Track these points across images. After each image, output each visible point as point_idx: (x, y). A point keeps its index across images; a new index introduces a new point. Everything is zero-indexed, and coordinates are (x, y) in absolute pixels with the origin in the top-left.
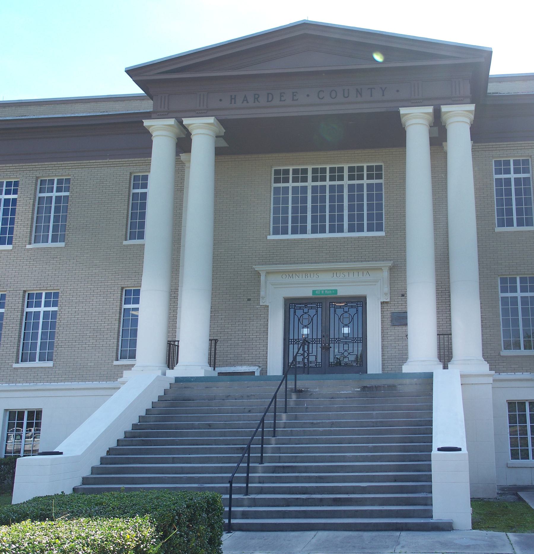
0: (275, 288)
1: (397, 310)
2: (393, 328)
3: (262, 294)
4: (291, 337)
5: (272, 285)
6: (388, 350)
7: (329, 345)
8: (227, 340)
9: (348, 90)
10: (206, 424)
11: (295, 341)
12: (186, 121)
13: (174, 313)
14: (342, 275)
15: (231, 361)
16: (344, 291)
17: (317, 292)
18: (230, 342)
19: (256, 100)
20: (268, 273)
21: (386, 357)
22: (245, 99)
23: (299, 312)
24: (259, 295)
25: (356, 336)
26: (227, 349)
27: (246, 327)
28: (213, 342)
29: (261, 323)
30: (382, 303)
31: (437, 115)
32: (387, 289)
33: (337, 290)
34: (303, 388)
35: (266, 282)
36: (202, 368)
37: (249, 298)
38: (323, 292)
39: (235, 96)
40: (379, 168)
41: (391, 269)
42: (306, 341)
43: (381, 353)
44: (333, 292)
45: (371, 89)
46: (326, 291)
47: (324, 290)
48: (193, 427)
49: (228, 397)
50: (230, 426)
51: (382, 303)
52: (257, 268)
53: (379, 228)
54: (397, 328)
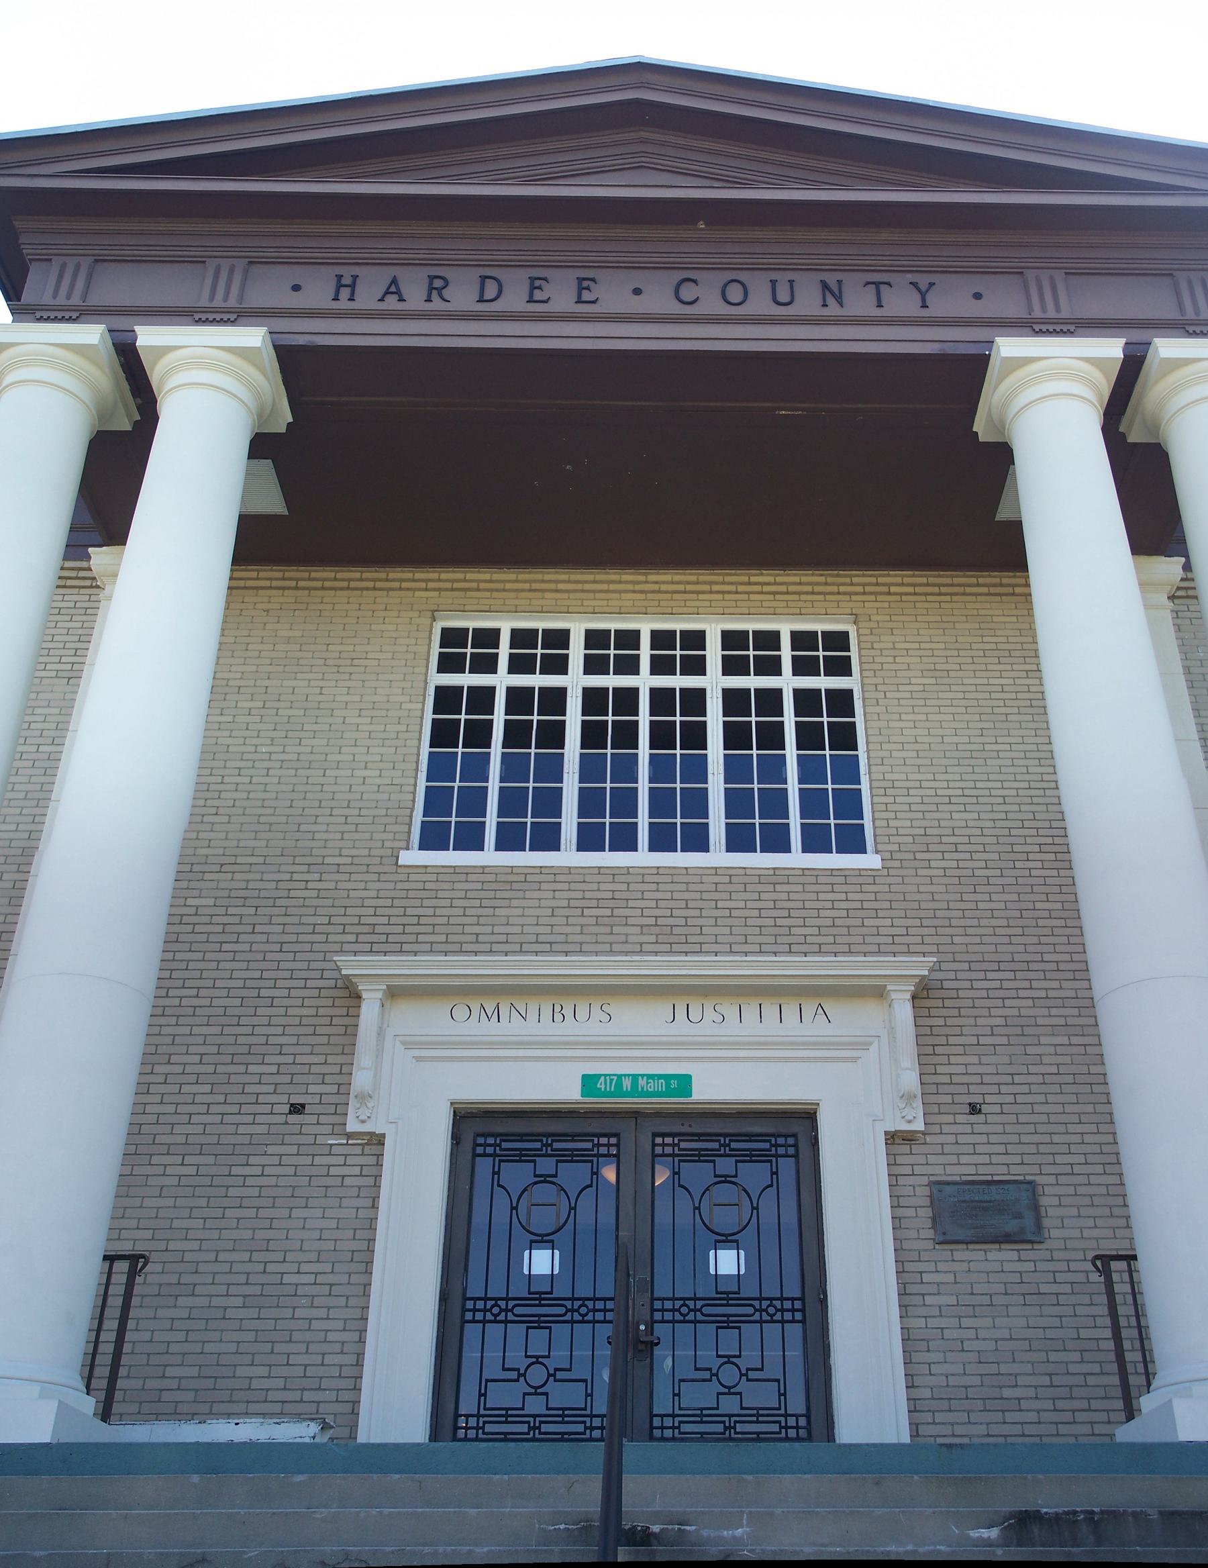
0: (418, 1059)
1: (955, 1173)
2: (943, 1252)
3: (361, 1079)
4: (475, 1290)
5: (408, 1046)
6: (931, 1357)
9: (791, 282)
12: (148, 337)
14: (710, 1015)
16: (720, 1083)
17: (601, 1085)
18: (190, 1301)
19: (435, 293)
20: (395, 993)
22: (393, 289)
23: (516, 1175)
24: (343, 1089)
25: (771, 1290)
26: (169, 1336)
28: (122, 1267)
29: (342, 1213)
30: (892, 1138)
31: (1132, 369)
32: (910, 1079)
35: (381, 1033)
37: (295, 1100)
38: (627, 1084)
39: (355, 278)
40: (838, 640)
44: (674, 1084)
45: (878, 284)
46: (642, 1082)
47: (635, 1077)
51: (892, 1138)
52: (351, 965)
53: (853, 842)
54: (961, 1253)
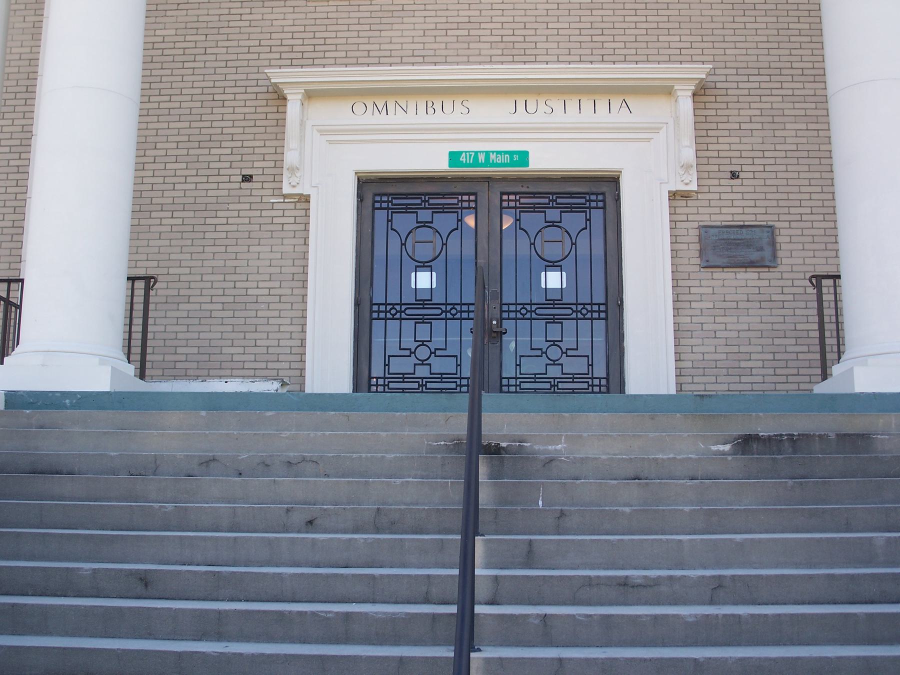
1: (717, 220)
2: (706, 274)
3: (290, 157)
5: (322, 133)
7: (500, 324)
8: (177, 300)
10: (131, 573)
11: (396, 311)
13: (13, 217)
14: (542, 107)
15: (187, 365)
17: (463, 159)
20: (310, 95)
21: (689, 364)
23: (404, 222)
24: (278, 164)
27: (236, 263)
28: (140, 285)
30: (674, 196)
33: (526, 153)
34: (504, 438)
35: (302, 124)
36: (102, 363)
38: (482, 158)
41: (701, 92)
42: (423, 309)
43: (672, 350)
47: (487, 153)
48: (68, 585)
49: (208, 463)
50: (240, 589)
51: (674, 196)
52: (278, 76)
54: (718, 274)
